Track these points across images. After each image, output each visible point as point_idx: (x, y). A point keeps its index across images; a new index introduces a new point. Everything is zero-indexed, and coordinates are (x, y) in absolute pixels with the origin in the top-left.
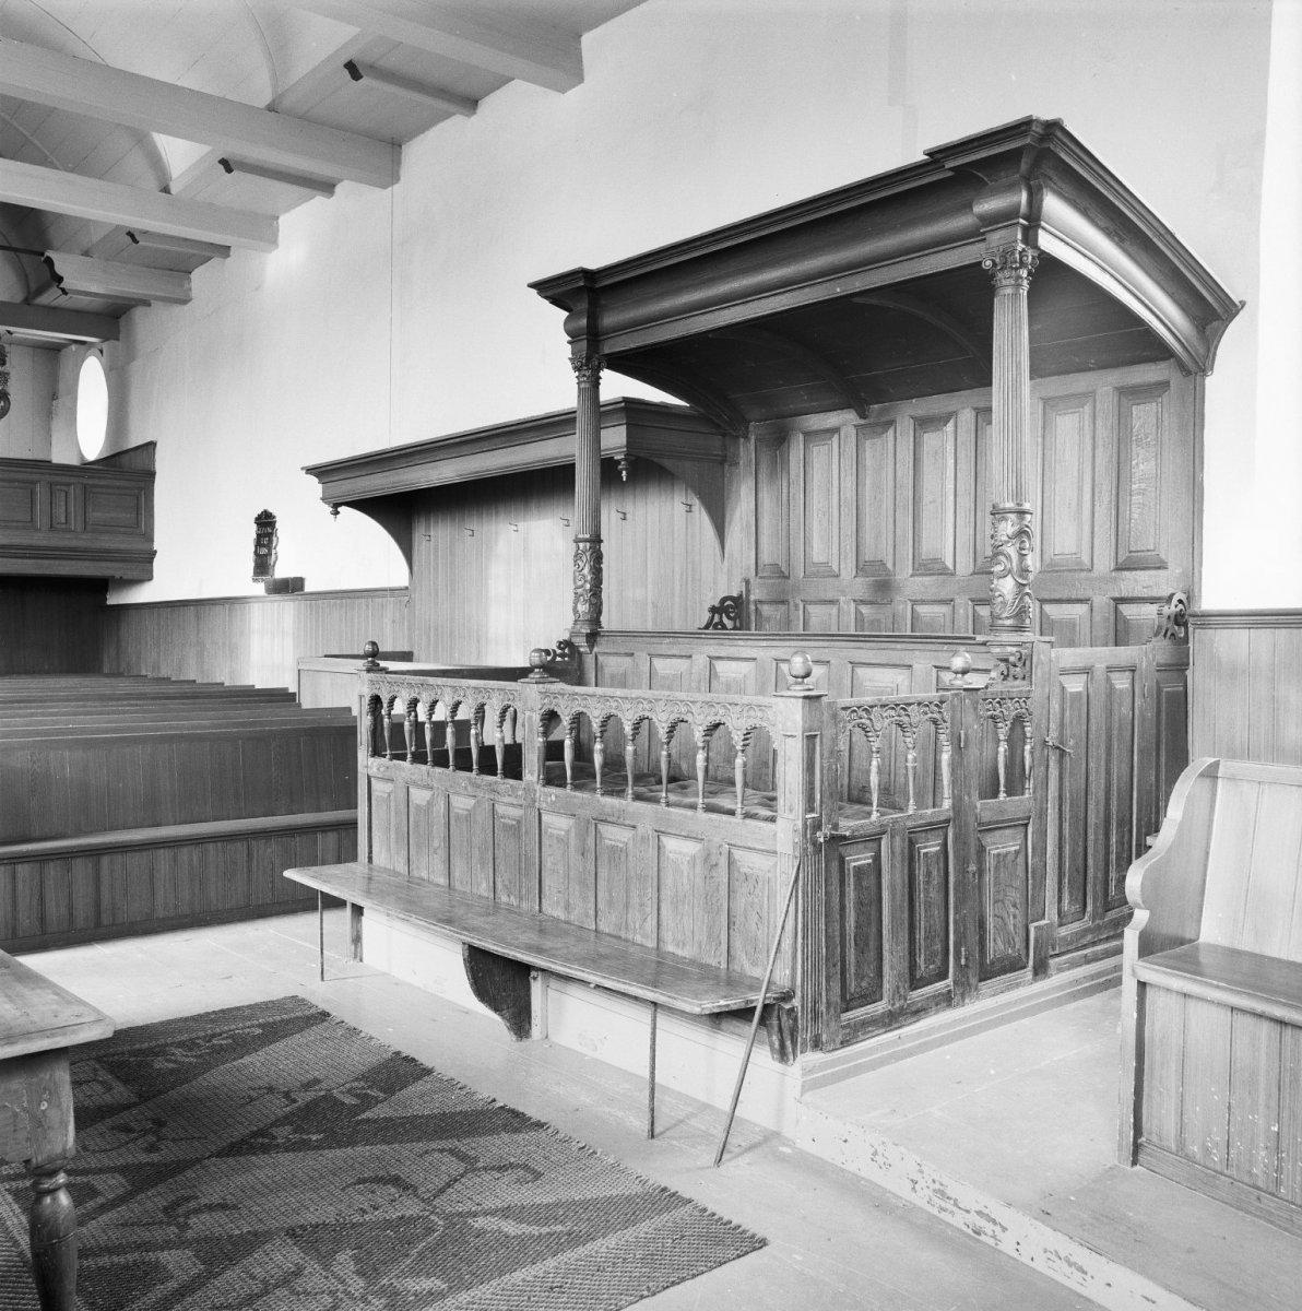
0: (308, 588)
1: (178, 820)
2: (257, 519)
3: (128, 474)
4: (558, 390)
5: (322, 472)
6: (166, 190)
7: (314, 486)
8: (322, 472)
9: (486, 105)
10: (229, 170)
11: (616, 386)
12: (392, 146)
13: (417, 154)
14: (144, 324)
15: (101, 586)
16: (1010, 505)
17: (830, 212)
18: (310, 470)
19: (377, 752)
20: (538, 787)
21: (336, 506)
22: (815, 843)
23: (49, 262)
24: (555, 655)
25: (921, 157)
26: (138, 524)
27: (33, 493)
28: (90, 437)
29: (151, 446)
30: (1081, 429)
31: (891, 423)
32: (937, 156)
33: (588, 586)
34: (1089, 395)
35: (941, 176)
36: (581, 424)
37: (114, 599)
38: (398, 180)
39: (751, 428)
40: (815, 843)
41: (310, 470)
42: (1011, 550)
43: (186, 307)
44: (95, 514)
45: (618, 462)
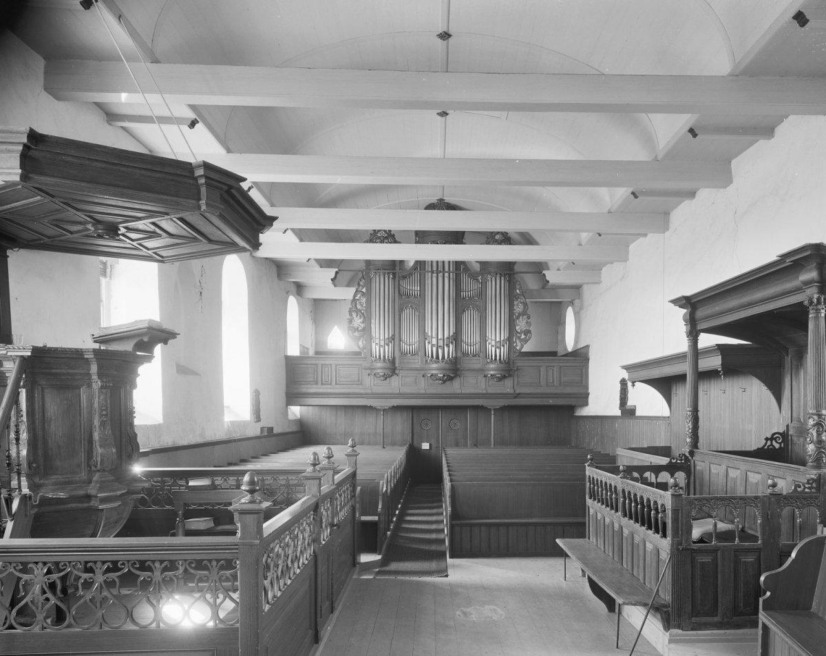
0: (638, 413)
2: (621, 381)
4: (683, 345)
6: (580, 245)
9: (779, 130)
10: (636, 197)
11: (707, 340)
12: (667, 214)
13: (739, 165)
14: (587, 291)
15: (572, 408)
17: (757, 276)
19: (591, 498)
20: (622, 518)
22: (678, 550)
23: (544, 275)
26: (582, 381)
33: (690, 431)
39: (789, 351)
40: (678, 550)
45: (720, 372)
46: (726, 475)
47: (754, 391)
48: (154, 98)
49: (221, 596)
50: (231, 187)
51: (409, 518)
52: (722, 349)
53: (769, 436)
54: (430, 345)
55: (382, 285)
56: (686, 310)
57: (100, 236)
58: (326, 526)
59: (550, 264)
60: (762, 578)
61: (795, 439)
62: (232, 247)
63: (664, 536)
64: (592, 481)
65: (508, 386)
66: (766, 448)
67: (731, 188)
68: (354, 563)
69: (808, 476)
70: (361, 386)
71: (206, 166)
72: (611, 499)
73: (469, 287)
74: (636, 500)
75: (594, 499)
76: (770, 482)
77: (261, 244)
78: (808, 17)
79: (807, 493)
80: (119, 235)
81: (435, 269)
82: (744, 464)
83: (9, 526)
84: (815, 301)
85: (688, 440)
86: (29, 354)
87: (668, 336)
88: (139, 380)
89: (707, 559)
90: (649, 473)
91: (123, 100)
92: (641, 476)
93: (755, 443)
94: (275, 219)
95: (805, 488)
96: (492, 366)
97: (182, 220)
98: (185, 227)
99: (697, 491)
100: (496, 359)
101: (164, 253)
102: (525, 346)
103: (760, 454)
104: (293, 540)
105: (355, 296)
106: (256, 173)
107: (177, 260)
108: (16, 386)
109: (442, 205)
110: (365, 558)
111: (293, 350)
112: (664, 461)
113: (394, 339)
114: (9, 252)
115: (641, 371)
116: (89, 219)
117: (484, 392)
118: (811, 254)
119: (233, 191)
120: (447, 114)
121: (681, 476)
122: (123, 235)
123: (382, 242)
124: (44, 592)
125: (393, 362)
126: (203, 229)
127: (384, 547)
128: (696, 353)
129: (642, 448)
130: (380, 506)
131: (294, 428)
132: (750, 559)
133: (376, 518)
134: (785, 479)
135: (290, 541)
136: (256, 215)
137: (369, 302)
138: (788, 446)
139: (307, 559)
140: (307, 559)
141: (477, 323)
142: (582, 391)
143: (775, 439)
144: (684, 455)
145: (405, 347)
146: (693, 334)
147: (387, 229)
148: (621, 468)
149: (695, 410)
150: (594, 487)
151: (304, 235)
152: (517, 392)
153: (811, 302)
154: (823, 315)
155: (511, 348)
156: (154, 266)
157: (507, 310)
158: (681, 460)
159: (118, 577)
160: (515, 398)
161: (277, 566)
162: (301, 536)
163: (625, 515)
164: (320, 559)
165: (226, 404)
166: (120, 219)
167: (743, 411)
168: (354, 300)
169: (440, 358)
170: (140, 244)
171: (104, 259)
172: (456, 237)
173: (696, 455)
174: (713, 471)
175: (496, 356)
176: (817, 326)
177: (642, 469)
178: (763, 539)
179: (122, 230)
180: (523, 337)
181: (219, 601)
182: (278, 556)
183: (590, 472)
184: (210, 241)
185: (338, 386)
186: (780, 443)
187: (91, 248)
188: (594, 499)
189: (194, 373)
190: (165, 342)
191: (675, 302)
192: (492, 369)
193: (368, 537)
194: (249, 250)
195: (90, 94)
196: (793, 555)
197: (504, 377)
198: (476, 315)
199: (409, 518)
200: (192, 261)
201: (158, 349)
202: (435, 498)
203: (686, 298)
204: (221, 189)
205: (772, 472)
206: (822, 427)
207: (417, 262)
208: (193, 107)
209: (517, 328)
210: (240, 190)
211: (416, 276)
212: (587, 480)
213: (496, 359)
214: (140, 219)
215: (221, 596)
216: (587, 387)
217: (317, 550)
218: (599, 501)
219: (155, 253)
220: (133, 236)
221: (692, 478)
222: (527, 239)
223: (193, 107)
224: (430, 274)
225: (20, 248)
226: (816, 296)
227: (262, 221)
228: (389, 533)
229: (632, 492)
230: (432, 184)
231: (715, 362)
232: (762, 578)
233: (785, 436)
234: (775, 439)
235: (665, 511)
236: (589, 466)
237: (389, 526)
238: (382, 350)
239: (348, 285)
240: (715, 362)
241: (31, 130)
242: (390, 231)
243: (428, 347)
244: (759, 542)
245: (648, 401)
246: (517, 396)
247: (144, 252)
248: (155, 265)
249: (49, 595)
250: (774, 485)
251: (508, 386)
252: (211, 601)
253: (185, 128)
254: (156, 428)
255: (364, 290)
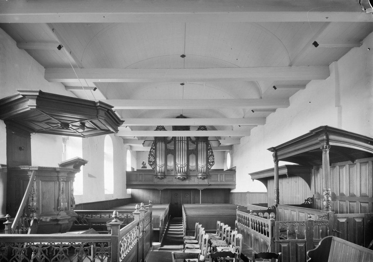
1: (188, 231)
3: (232, 171)
4: (272, 165)
5: (252, 174)
7: (250, 177)
8: (252, 174)
9: (307, 86)
11: (282, 163)
12: (265, 118)
13: (268, 119)
15: (230, 190)
16: (325, 189)
18: (249, 174)
21: (253, 180)
23: (219, 141)
24: (271, 208)
25: (308, 132)
27: (218, 176)
28: (228, 166)
29: (235, 167)
30: (366, 169)
31: (335, 167)
32: (312, 131)
33: (276, 197)
34: (367, 162)
35: (312, 134)
36: (275, 170)
37: (232, 191)
38: (265, 123)
41: (249, 174)
42: (325, 197)
43: (240, 145)
44: (227, 179)
45: (287, 175)
46: (287, 213)
47: (299, 182)
48: (82, 80)
49: (105, 256)
50: (109, 110)
51: (170, 229)
52: (288, 167)
53: (307, 199)
54: (178, 167)
55: (161, 146)
56: (273, 153)
57: (63, 128)
58: (141, 232)
59: (222, 138)
60: (308, 253)
61: (317, 200)
62: (108, 132)
63: (268, 236)
64: (239, 215)
65: (206, 182)
66: (305, 203)
67: (289, 108)
68: (151, 246)
69: (323, 214)
70: (152, 182)
71: (100, 102)
72: (247, 223)
73: (192, 147)
74: (256, 223)
75: (240, 223)
76: (309, 216)
77: (118, 131)
78: (318, 43)
79: (323, 220)
80: (69, 127)
81: (179, 139)
82: (297, 209)
83: (29, 230)
84: (325, 147)
85: (275, 201)
86: (37, 169)
87: (267, 162)
88: (75, 179)
89: (286, 245)
90: (260, 213)
91: (71, 81)
92: (258, 214)
93: (302, 202)
94: (123, 121)
95: (322, 218)
96: (200, 174)
97: (91, 121)
98: (92, 124)
99: (279, 220)
100: (202, 172)
101: (85, 134)
102: (212, 167)
103: (303, 206)
104: (127, 239)
105: (151, 150)
106: (117, 107)
107: (89, 136)
108: (33, 180)
109: (182, 117)
110: (154, 244)
111: (129, 169)
112: (266, 208)
113: (166, 164)
114: (31, 134)
115: (256, 176)
116: (59, 122)
117: (197, 184)
118: (323, 130)
119: (109, 111)
120: (184, 84)
121: (272, 215)
122: (71, 128)
123: (160, 130)
124: (41, 254)
125: (164, 173)
126: (99, 125)
127: (162, 240)
128: (278, 168)
129: (258, 204)
130: (160, 225)
131: (130, 197)
132: (302, 245)
133: (159, 229)
134: (314, 216)
135: (129, 236)
136: (117, 120)
137: (156, 152)
138: (314, 203)
139: (135, 243)
140: (135, 243)
141: (195, 159)
142: (234, 183)
143: (309, 200)
144: (274, 206)
145: (168, 168)
146: (276, 161)
147: (162, 125)
148: (251, 211)
149: (278, 190)
150: (240, 218)
151: (132, 128)
152: (210, 184)
153: (323, 148)
154: (328, 153)
155: (207, 168)
156: (80, 139)
157: (206, 153)
158: (273, 208)
159: (68, 248)
160: (209, 186)
161: (124, 245)
162: (132, 234)
163: (252, 229)
164: (139, 244)
165: (105, 188)
166: (70, 122)
167: (295, 190)
168: (150, 152)
169: (181, 172)
170: (76, 131)
171: (63, 136)
172: (187, 128)
173: (278, 206)
174: (285, 212)
175: (202, 171)
176: (326, 157)
177: (257, 212)
178: (307, 238)
179: (71, 126)
180: (211, 164)
181: (103, 258)
182: (125, 242)
183: (238, 212)
184: (101, 130)
185: (144, 182)
186: (311, 202)
187: (61, 132)
188: (240, 223)
189: (95, 177)
190: (84, 164)
191: (269, 149)
192: (200, 175)
193: (155, 236)
194: (114, 133)
195: (59, 79)
196: (320, 244)
197: (204, 178)
198: (194, 156)
199: (170, 229)
200: (94, 137)
201: (82, 167)
202: (180, 222)
203: (273, 148)
204: (105, 110)
205: (309, 212)
206: (329, 195)
207: (173, 137)
208: (95, 83)
209: (209, 160)
210: (112, 111)
211: (173, 142)
212: (237, 215)
213: (202, 172)
214: (77, 122)
215: (105, 256)
216: (235, 182)
217: (138, 240)
218: (242, 223)
219: (82, 134)
220: (74, 128)
221: (277, 214)
222: (213, 128)
223: (95, 83)
224: (178, 141)
225: (36, 132)
226: (325, 145)
227: (120, 123)
228: (163, 235)
229: (255, 220)
230: (178, 108)
231: (285, 171)
232: (308, 253)
233: (312, 199)
234: (309, 200)
235: (268, 226)
236: (238, 210)
237: (163, 232)
238: (160, 169)
239: (148, 146)
240: (285, 171)
241: (40, 91)
242: (163, 126)
243: (177, 168)
244: (305, 239)
245: (260, 187)
246: (210, 185)
247: (78, 134)
248: (81, 138)
249: (43, 255)
250: (310, 217)
251: (206, 182)
252: (101, 258)
253: (92, 91)
254: (80, 196)
255: (154, 148)
